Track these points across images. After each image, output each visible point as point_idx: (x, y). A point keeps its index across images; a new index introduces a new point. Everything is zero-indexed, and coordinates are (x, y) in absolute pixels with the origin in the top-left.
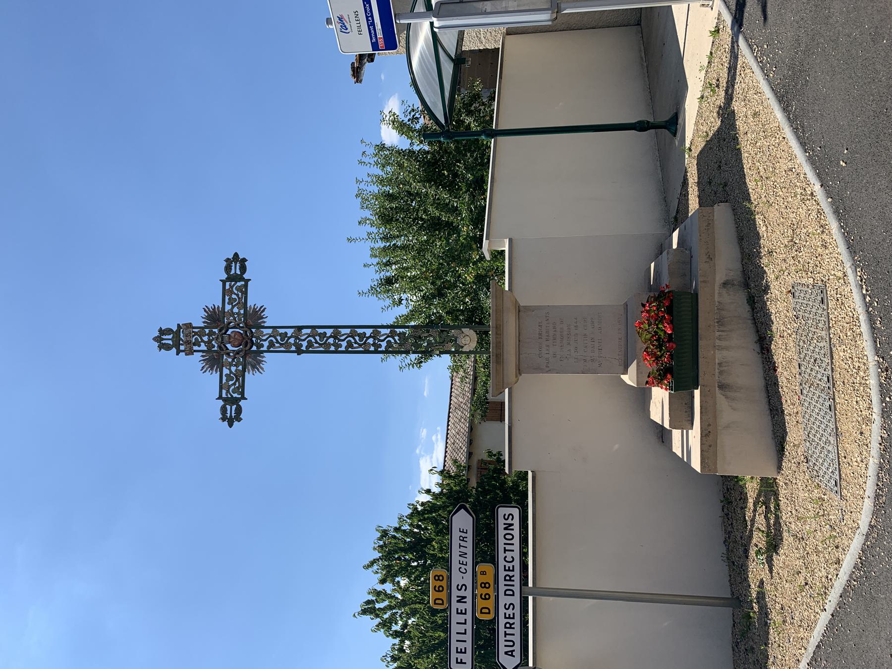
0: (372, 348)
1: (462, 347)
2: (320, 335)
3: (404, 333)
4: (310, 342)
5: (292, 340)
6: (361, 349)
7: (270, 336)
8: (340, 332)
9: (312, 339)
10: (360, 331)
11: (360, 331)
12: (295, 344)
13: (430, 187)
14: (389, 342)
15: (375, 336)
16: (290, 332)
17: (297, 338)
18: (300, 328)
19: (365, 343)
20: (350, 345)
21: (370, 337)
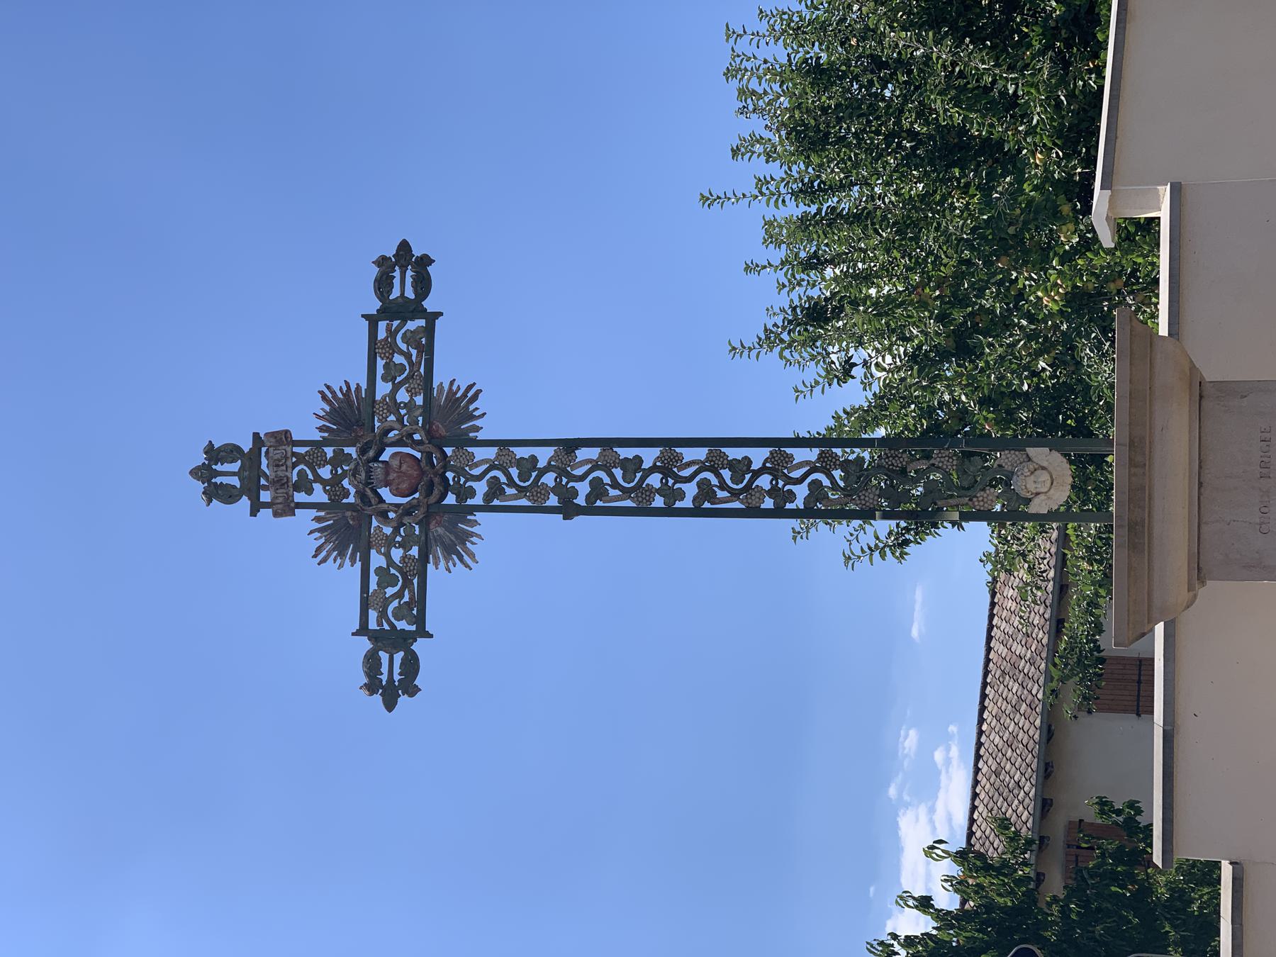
0: (768, 503)
1: (1028, 501)
2: (624, 464)
5: (764, 481)
6: (737, 505)
7: (814, 470)
8: (679, 457)
11: (734, 453)
15: (777, 467)
16: (544, 455)
17: (562, 472)
18: (570, 446)
19: (748, 488)
20: (706, 491)
21: (763, 470)
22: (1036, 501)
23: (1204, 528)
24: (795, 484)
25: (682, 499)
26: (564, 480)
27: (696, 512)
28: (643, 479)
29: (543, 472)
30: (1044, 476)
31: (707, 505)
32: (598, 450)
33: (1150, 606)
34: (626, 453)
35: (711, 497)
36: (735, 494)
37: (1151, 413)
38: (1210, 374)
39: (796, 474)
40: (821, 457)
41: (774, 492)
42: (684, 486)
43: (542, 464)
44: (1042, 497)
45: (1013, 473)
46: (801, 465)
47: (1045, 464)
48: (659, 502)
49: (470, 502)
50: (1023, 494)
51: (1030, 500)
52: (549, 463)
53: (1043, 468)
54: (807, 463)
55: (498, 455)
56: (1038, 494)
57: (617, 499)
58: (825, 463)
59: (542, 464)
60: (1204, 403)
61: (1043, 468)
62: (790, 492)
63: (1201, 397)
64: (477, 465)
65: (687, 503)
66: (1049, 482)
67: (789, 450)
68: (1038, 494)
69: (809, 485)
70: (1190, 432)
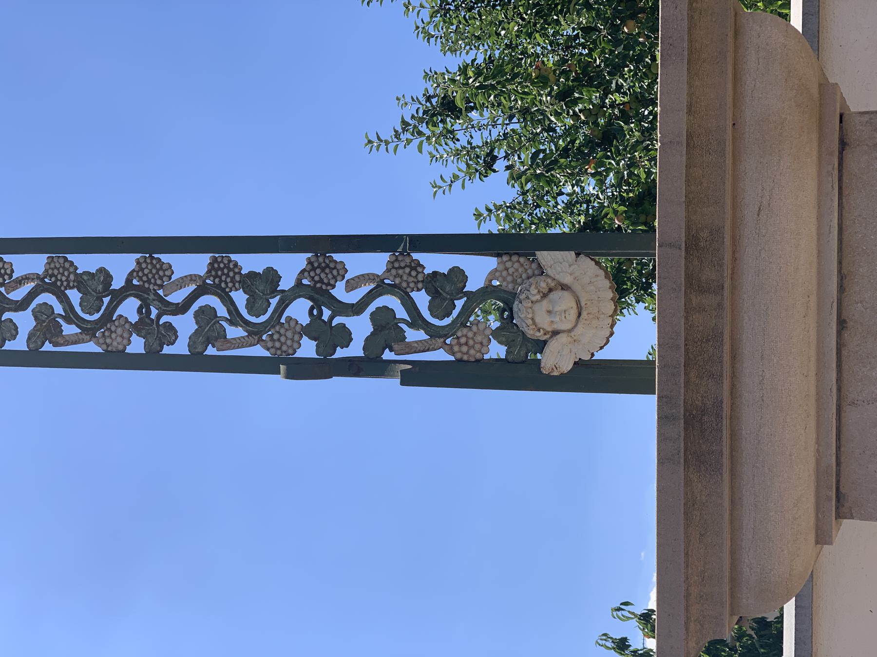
0: (137, 345)
1: (541, 346)
2: (249, 282)
3: (458, 275)
4: (384, 322)
5: (129, 309)
6: (91, 347)
7: (381, 289)
8: (340, 271)
9: (211, 300)
10: (86, 263)
11: (251, 263)
12: (143, 326)
13: (579, 15)
14: (206, 313)
15: (147, 286)
16: (121, 266)
17: (320, 295)
18: (323, 248)
19: (107, 317)
20: (47, 326)
21: (299, 290)
22: (553, 346)
23: (852, 415)
24: (174, 313)
25: (14, 337)
26: (327, 313)
27: (195, 362)
28: (467, 311)
29: (287, 299)
30: (564, 302)
31: (48, 347)
32: (386, 257)
33: (735, 582)
34: (435, 262)
35: (220, 337)
36: (255, 333)
37: (736, 179)
38: (858, 101)
39: (177, 297)
40: (213, 267)
41: (143, 326)
42: (350, 322)
43: (474, 284)
44: (562, 338)
45: (514, 295)
46: (21, 281)
47: (567, 280)
48: (308, 349)
49: (167, 350)
50: (531, 333)
51: (545, 342)
52: (129, 281)
53: (564, 287)
54: (192, 278)
55: (391, 266)
56: (555, 333)
57: (240, 343)
58: (220, 280)
59: (287, 283)
60: (848, 155)
61: (564, 287)
62: (169, 326)
63: (843, 144)
64: (21, 281)
65: (355, 350)
66: (573, 313)
67: (165, 258)
68: (555, 333)
69: (373, 315)
70: (820, 217)
